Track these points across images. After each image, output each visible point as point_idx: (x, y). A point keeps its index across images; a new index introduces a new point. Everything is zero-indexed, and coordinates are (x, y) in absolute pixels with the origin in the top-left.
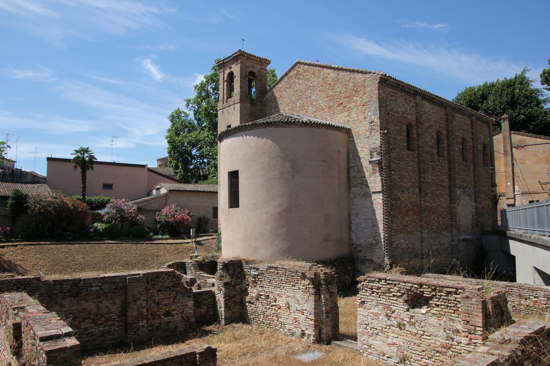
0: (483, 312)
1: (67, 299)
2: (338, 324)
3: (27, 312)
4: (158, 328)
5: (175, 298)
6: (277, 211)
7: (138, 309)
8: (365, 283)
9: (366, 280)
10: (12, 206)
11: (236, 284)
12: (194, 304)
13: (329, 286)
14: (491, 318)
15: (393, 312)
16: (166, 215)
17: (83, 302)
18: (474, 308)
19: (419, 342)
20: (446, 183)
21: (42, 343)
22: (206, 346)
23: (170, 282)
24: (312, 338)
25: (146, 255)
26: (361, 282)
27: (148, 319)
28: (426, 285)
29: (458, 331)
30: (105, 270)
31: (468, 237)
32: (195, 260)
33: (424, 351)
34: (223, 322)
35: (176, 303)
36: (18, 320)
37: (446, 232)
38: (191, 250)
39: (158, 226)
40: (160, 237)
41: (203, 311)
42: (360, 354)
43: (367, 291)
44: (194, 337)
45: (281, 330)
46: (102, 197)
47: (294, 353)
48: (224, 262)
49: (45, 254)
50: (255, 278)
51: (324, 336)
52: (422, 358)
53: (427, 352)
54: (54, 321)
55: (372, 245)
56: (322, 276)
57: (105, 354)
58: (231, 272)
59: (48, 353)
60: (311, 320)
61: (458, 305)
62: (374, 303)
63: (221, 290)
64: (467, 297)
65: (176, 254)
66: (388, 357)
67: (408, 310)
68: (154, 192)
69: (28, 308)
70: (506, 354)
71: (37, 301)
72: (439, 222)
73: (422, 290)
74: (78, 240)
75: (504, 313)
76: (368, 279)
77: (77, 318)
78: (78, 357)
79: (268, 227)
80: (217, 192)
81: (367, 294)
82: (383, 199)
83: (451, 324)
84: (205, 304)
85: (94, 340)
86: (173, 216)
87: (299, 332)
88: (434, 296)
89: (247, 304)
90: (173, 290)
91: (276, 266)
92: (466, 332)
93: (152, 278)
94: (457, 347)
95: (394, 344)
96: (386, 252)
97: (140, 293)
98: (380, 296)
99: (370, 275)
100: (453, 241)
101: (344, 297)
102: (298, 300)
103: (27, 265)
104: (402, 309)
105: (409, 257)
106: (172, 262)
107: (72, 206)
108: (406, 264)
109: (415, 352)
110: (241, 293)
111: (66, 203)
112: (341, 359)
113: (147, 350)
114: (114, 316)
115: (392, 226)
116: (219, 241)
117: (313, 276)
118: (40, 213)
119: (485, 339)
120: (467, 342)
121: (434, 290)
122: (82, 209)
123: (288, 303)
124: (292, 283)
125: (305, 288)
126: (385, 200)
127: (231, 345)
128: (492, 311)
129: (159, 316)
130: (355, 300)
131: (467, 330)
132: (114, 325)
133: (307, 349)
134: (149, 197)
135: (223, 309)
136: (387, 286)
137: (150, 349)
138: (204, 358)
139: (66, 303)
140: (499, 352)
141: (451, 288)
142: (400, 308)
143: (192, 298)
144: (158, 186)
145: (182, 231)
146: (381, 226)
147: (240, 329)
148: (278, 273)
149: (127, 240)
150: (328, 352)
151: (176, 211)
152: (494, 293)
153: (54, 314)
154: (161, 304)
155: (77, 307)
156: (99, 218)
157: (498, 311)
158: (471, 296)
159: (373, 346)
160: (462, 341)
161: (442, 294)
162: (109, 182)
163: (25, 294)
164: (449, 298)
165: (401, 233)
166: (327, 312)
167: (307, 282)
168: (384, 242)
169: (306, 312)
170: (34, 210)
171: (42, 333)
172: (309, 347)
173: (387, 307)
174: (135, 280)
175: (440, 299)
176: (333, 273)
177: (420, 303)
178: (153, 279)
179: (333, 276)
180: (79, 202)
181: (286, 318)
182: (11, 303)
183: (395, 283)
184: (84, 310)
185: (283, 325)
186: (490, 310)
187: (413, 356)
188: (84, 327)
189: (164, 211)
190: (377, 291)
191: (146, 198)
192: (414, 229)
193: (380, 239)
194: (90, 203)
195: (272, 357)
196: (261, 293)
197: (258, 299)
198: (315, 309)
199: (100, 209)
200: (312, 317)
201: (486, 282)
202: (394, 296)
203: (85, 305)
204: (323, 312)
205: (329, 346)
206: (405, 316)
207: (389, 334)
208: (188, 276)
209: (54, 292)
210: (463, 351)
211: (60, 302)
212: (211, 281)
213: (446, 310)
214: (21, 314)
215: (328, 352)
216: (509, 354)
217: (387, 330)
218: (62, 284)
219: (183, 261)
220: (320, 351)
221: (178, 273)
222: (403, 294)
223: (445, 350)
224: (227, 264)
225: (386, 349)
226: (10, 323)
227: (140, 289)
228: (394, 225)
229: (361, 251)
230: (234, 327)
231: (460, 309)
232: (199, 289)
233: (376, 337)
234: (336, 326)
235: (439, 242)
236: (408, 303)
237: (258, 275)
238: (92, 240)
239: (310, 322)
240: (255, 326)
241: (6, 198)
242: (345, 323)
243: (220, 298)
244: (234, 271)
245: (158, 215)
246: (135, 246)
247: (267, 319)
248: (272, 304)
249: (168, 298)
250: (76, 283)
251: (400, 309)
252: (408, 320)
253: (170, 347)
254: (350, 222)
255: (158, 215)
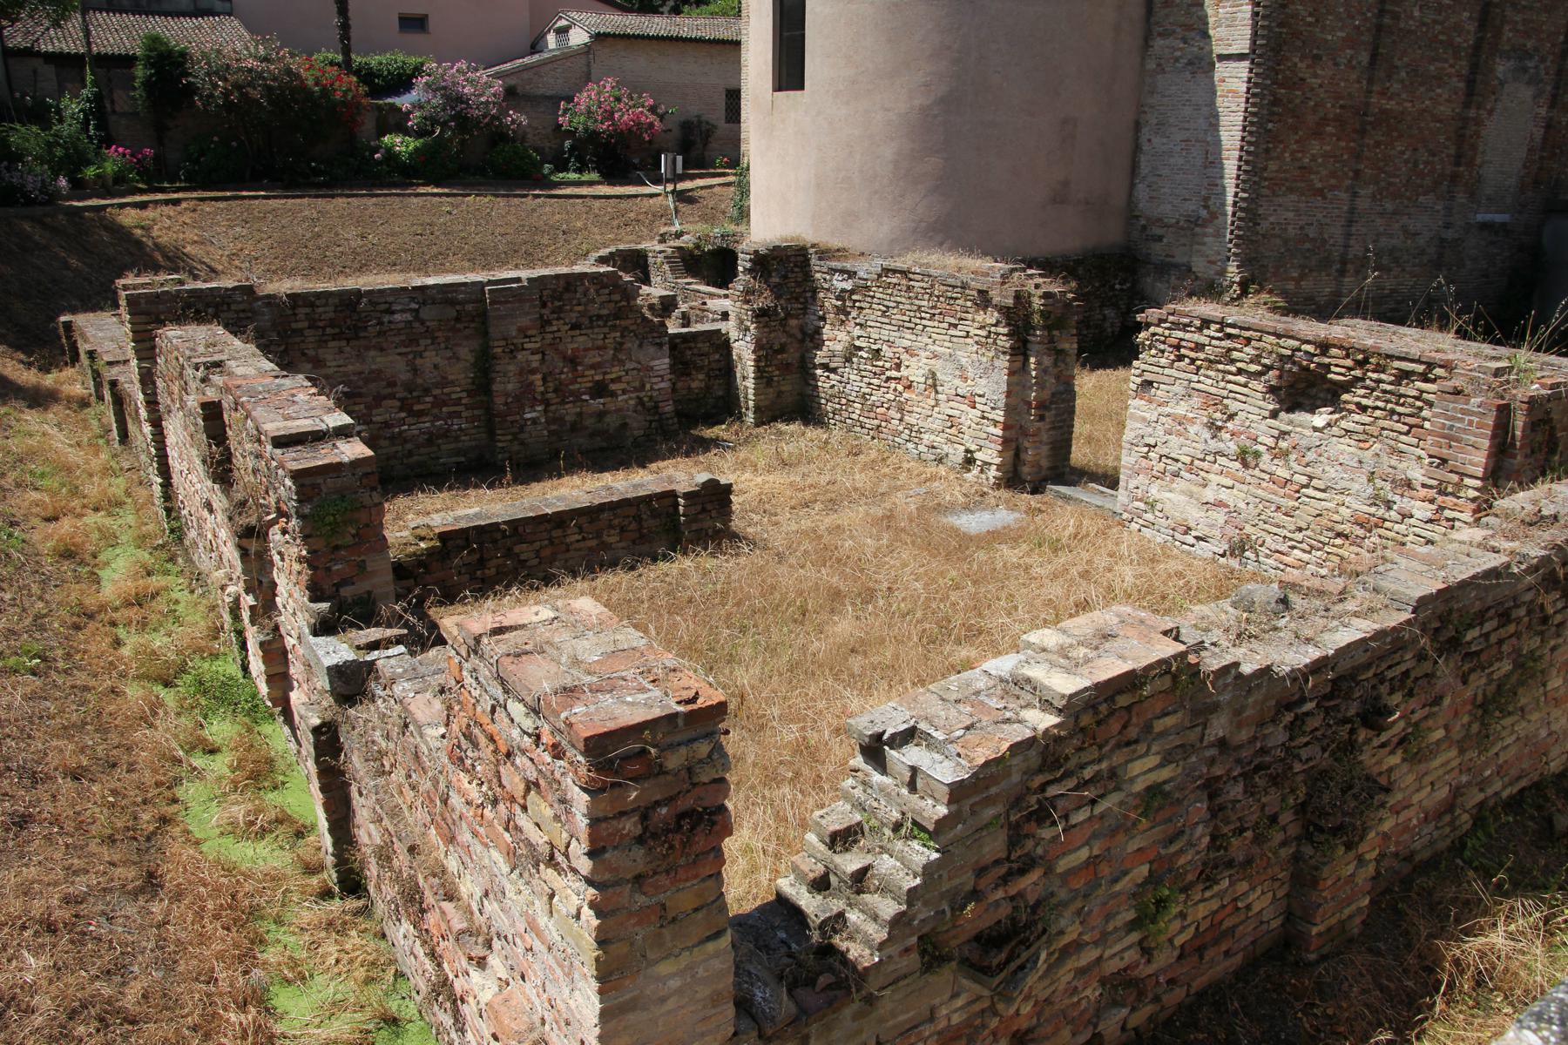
0: (1494, 437)
1: (331, 344)
2: (1070, 440)
3: (230, 374)
4: (575, 428)
5: (619, 347)
6: (917, 102)
7: (520, 374)
8: (1159, 330)
9: (1165, 321)
10: (147, 84)
11: (788, 315)
12: (672, 366)
13: (1056, 333)
14: (1514, 456)
15: (1231, 417)
16: (589, 112)
17: (372, 353)
18: (1470, 423)
19: (1292, 503)
20: (1466, 40)
21: (278, 451)
22: (703, 477)
23: (602, 305)
24: (993, 472)
25: (536, 230)
26: (1148, 325)
27: (547, 403)
28: (1341, 347)
29: (1408, 484)
30: (423, 269)
31: (1499, 218)
32: (672, 243)
33: (1300, 530)
34: (750, 418)
35: (622, 363)
36: (211, 394)
37: (1431, 196)
38: (663, 215)
39: (567, 144)
40: (573, 176)
41: (694, 385)
42: (1122, 524)
43: (1163, 352)
44: (672, 454)
45: (910, 445)
46: (401, 58)
47: (941, 509)
48: (756, 252)
49: (256, 226)
50: (844, 300)
51: (1026, 469)
52: (1293, 548)
53: (1308, 533)
54: (301, 397)
55: (1195, 222)
56: (1037, 303)
57: (441, 491)
58: (775, 280)
59: (297, 476)
60: (995, 423)
61: (1425, 413)
62: (1178, 388)
63: (747, 329)
64: (1457, 392)
65: (619, 227)
66: (1197, 538)
67: (1274, 415)
68: (551, 40)
69: (232, 363)
70: (1533, 553)
71: (251, 348)
72: (1416, 164)
73: (1327, 360)
74: (343, 187)
75: (1556, 445)
76: (1171, 318)
77: (360, 395)
78: (373, 489)
79: (888, 152)
80: (738, 43)
81: (1163, 361)
82: (1249, 81)
83: (1393, 463)
84: (702, 368)
85: (410, 454)
86: (610, 115)
87: (958, 455)
88: (1357, 379)
89: (819, 372)
90: (615, 326)
91: (905, 267)
92: (1431, 487)
93: (554, 291)
94: (1397, 527)
95: (1220, 504)
96: (1236, 245)
97: (523, 332)
98: (1199, 368)
99: (1179, 307)
100: (1447, 226)
101: (1093, 369)
102: (961, 368)
103: (216, 257)
104: (1257, 411)
105: (1302, 267)
106: (608, 250)
107: (317, 84)
108: (1291, 286)
109: (1275, 530)
110: (802, 341)
111: (298, 76)
112: (1067, 533)
113: (548, 484)
114: (457, 392)
115: (1265, 169)
116: (744, 191)
117: (1010, 302)
118: (229, 106)
119: (1482, 508)
120: (1429, 515)
121: (1361, 364)
122: (345, 93)
123: (934, 374)
124: (948, 319)
125: (984, 333)
126: (1256, 85)
127: (771, 478)
128: (1523, 437)
129: (577, 396)
130: (1126, 380)
131: (1435, 483)
132: (458, 415)
133: (976, 501)
134: (536, 57)
135: (750, 383)
136: (1223, 343)
137: (555, 482)
138: (699, 508)
139: (328, 354)
140: (1515, 545)
141: (1412, 361)
142: (1252, 408)
143: (666, 348)
144: (563, 23)
145: (636, 161)
146: (1231, 167)
147: (796, 437)
148: (909, 288)
149: (481, 184)
150: (1031, 511)
151: (618, 99)
152: (1543, 386)
153: (300, 379)
154: (580, 364)
155: (358, 367)
156: (396, 121)
157: (1539, 438)
158: (1468, 389)
159: (1159, 506)
160: (1414, 512)
161: (1383, 376)
162: (417, 10)
163: (220, 330)
164: (1402, 390)
165: (1291, 190)
166: (1042, 406)
167: (992, 317)
168: (1234, 214)
169: (983, 400)
170: (211, 96)
171: (275, 426)
172: (983, 494)
173: (1215, 401)
174: (509, 294)
175: (1373, 390)
176: (1070, 296)
177: (1315, 397)
178: (558, 293)
179: (1068, 305)
180: (335, 71)
181: (926, 415)
182: (188, 353)
183: (1248, 334)
184: (376, 375)
185: (915, 433)
186: (1518, 433)
187: (1268, 540)
188: (378, 419)
189: (584, 99)
190: (1192, 354)
191: (527, 60)
192: (1333, 182)
193: (1224, 204)
194: (367, 76)
195: (880, 513)
196: (857, 343)
197: (848, 360)
198: (1009, 394)
199: (398, 94)
200: (999, 415)
201: (1523, 356)
202: (1240, 372)
203: (375, 360)
204: (1029, 404)
205: (1038, 497)
206: (1264, 432)
207: (1211, 476)
208: (655, 291)
209: (294, 326)
210: (1411, 537)
211: (311, 353)
212: (717, 304)
213: (1386, 423)
214: (217, 379)
215: (1031, 511)
216: (1543, 553)
217: (1205, 465)
218: (312, 305)
219: (639, 247)
220: (1013, 508)
221: (627, 278)
222: (1268, 368)
223: (1361, 532)
224: (764, 256)
225: (1194, 515)
226: (192, 401)
227: (524, 321)
228: (1273, 166)
229: (1160, 238)
230: (780, 433)
231: (1427, 425)
232: (684, 326)
233: (1172, 481)
234: (1062, 445)
235: (1405, 229)
236: (1278, 396)
237: (852, 292)
238: (382, 186)
239: (992, 430)
240: (837, 433)
241: (127, 61)
242: (1090, 440)
243: (744, 352)
244: (785, 277)
245: (566, 111)
246: (502, 202)
247: (872, 415)
248: (888, 373)
249: (599, 348)
250: (350, 300)
251: (1251, 409)
252: (1270, 442)
253: (607, 478)
254: (1137, 149)
255: (566, 111)
